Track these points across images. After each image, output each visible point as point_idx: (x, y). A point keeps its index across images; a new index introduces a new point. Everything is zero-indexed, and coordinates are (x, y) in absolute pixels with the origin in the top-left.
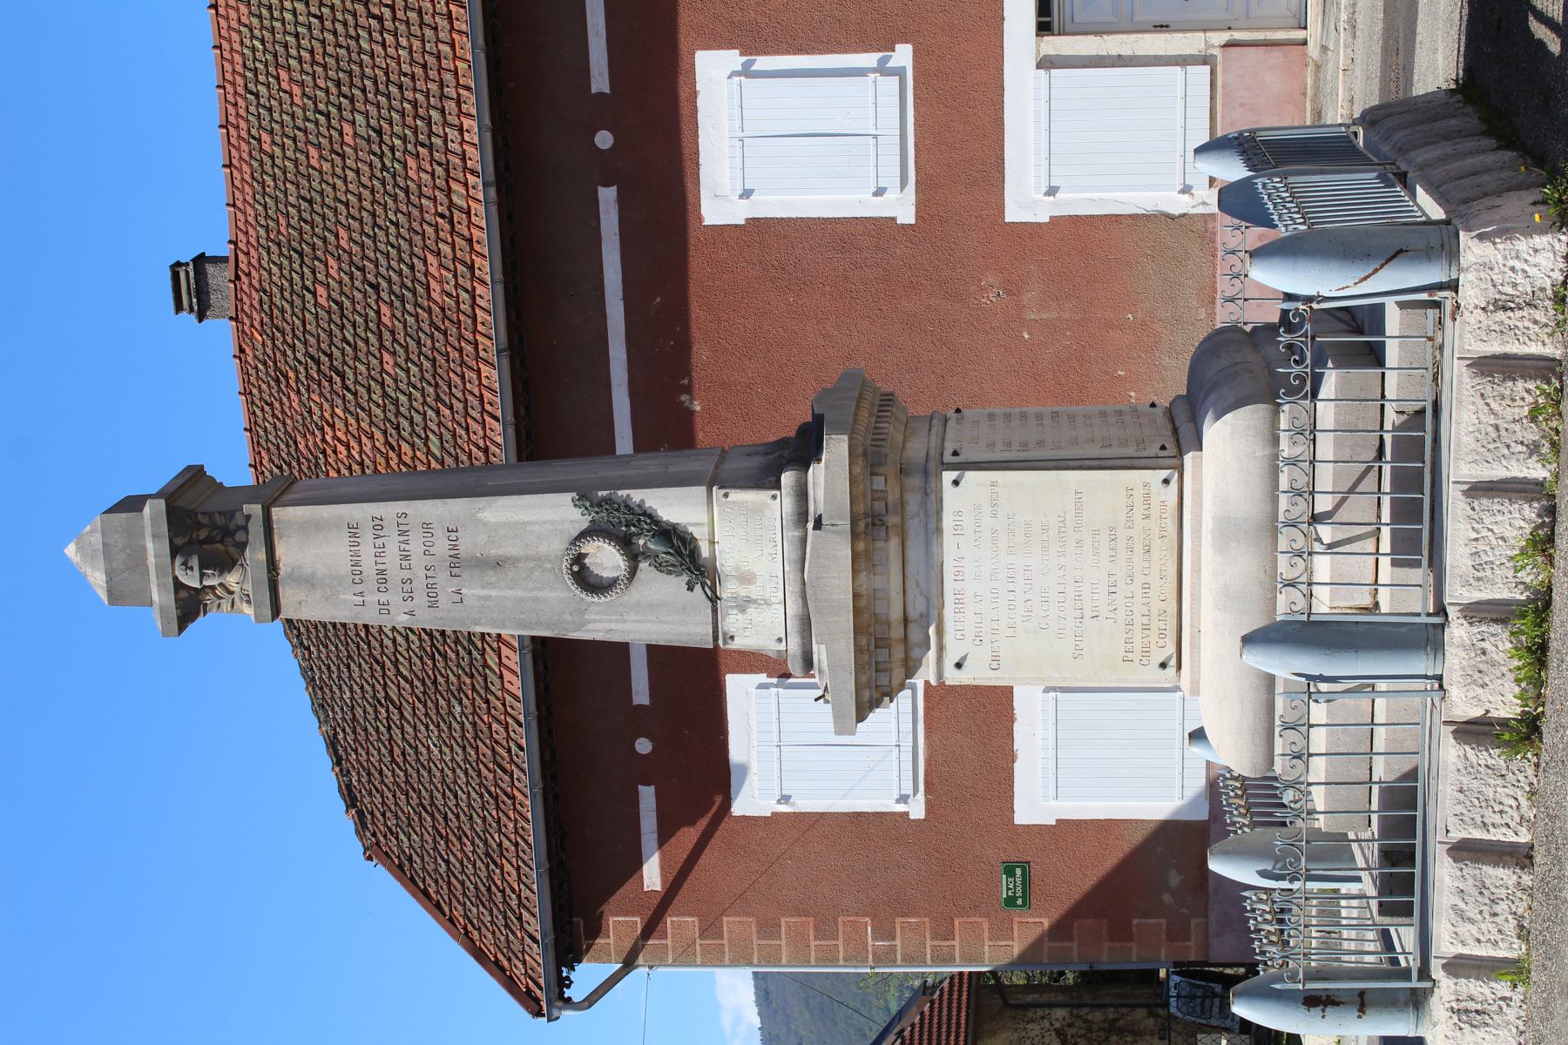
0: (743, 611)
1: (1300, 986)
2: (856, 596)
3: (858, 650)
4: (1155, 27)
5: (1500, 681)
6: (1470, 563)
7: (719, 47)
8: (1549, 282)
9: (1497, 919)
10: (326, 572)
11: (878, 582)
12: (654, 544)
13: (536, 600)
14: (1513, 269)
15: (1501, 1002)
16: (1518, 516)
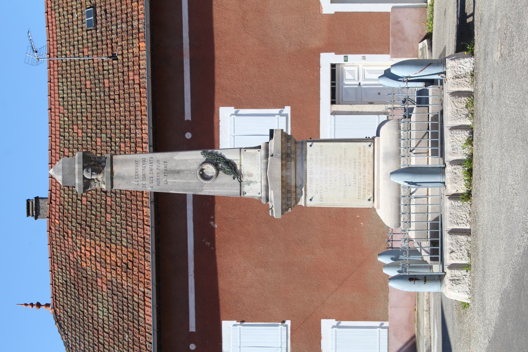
0: (249, 185)
1: (408, 274)
2: (282, 177)
3: (282, 193)
4: (369, 103)
5: (460, 182)
6: (451, 148)
7: (228, 106)
8: (469, 70)
9: (462, 251)
10: (128, 175)
11: (288, 174)
12: (224, 165)
13: (189, 183)
14: (460, 67)
15: (464, 276)
16: (463, 134)
